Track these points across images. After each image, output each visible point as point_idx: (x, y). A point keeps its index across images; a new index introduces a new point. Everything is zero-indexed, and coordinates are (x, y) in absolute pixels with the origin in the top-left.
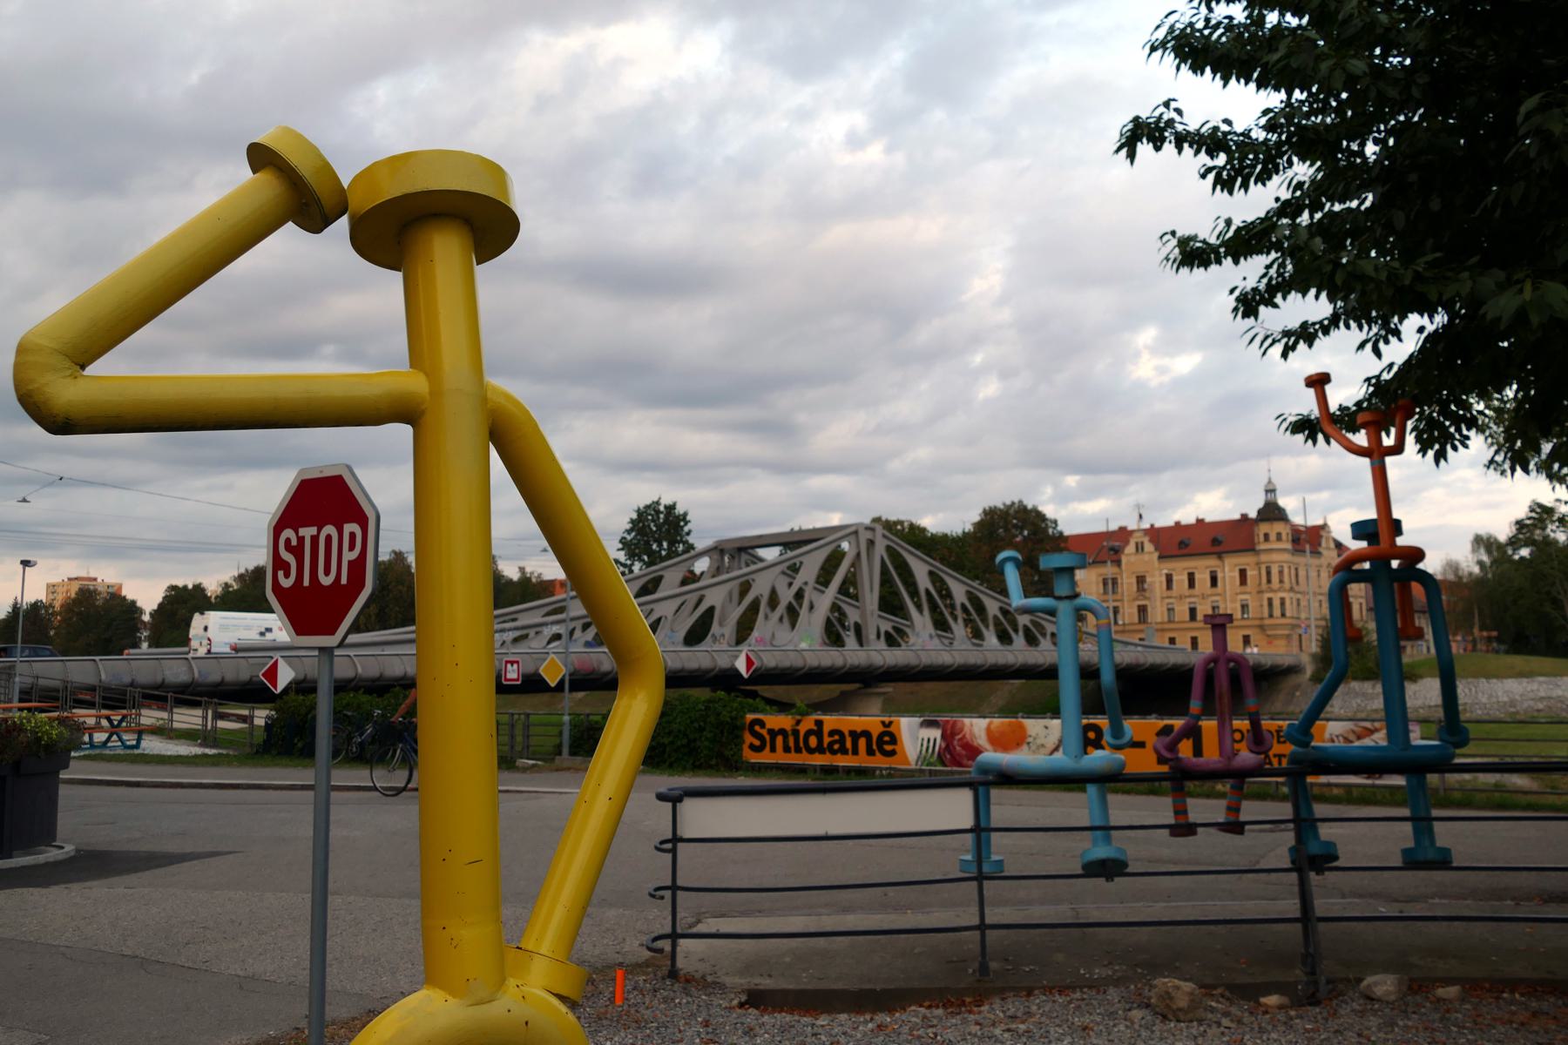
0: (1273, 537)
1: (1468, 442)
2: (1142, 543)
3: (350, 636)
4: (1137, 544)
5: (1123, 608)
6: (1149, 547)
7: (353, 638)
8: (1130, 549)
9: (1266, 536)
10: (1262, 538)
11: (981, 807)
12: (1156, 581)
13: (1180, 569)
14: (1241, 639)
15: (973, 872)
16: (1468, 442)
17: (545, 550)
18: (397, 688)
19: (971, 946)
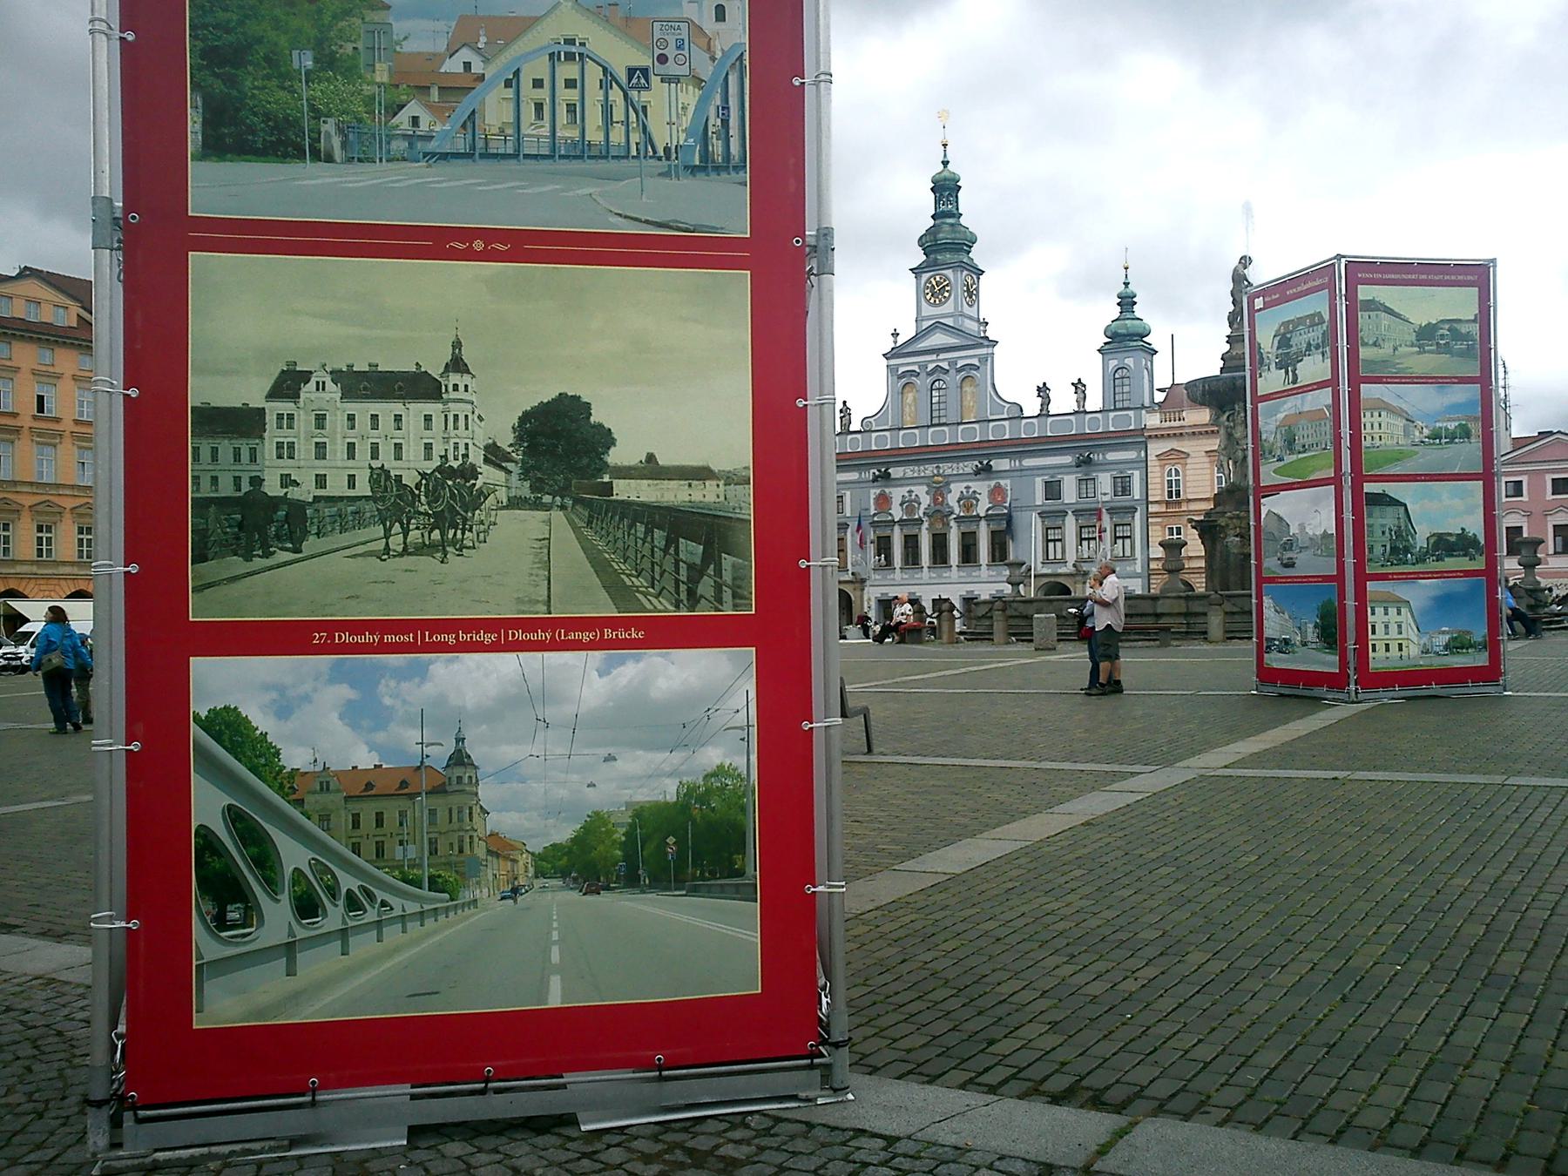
0: (462, 388)
1: (1041, 386)
2: (324, 383)
3: (685, 566)
4: (318, 383)
5: (299, 444)
6: (330, 385)
7: (649, 606)
8: (312, 385)
9: (456, 387)
10: (450, 388)
11: (1120, 537)
12: (336, 421)
13: (363, 410)
14: (209, 479)
15: (1467, 454)
16: (1041, 386)
17: (895, 334)
18: (551, 1150)
19: (739, 863)
